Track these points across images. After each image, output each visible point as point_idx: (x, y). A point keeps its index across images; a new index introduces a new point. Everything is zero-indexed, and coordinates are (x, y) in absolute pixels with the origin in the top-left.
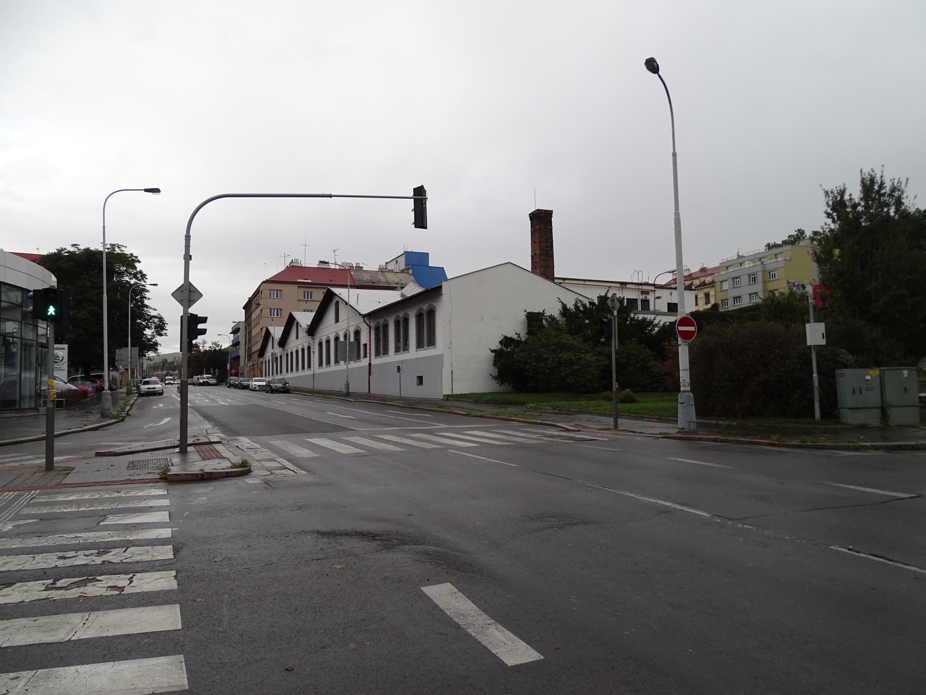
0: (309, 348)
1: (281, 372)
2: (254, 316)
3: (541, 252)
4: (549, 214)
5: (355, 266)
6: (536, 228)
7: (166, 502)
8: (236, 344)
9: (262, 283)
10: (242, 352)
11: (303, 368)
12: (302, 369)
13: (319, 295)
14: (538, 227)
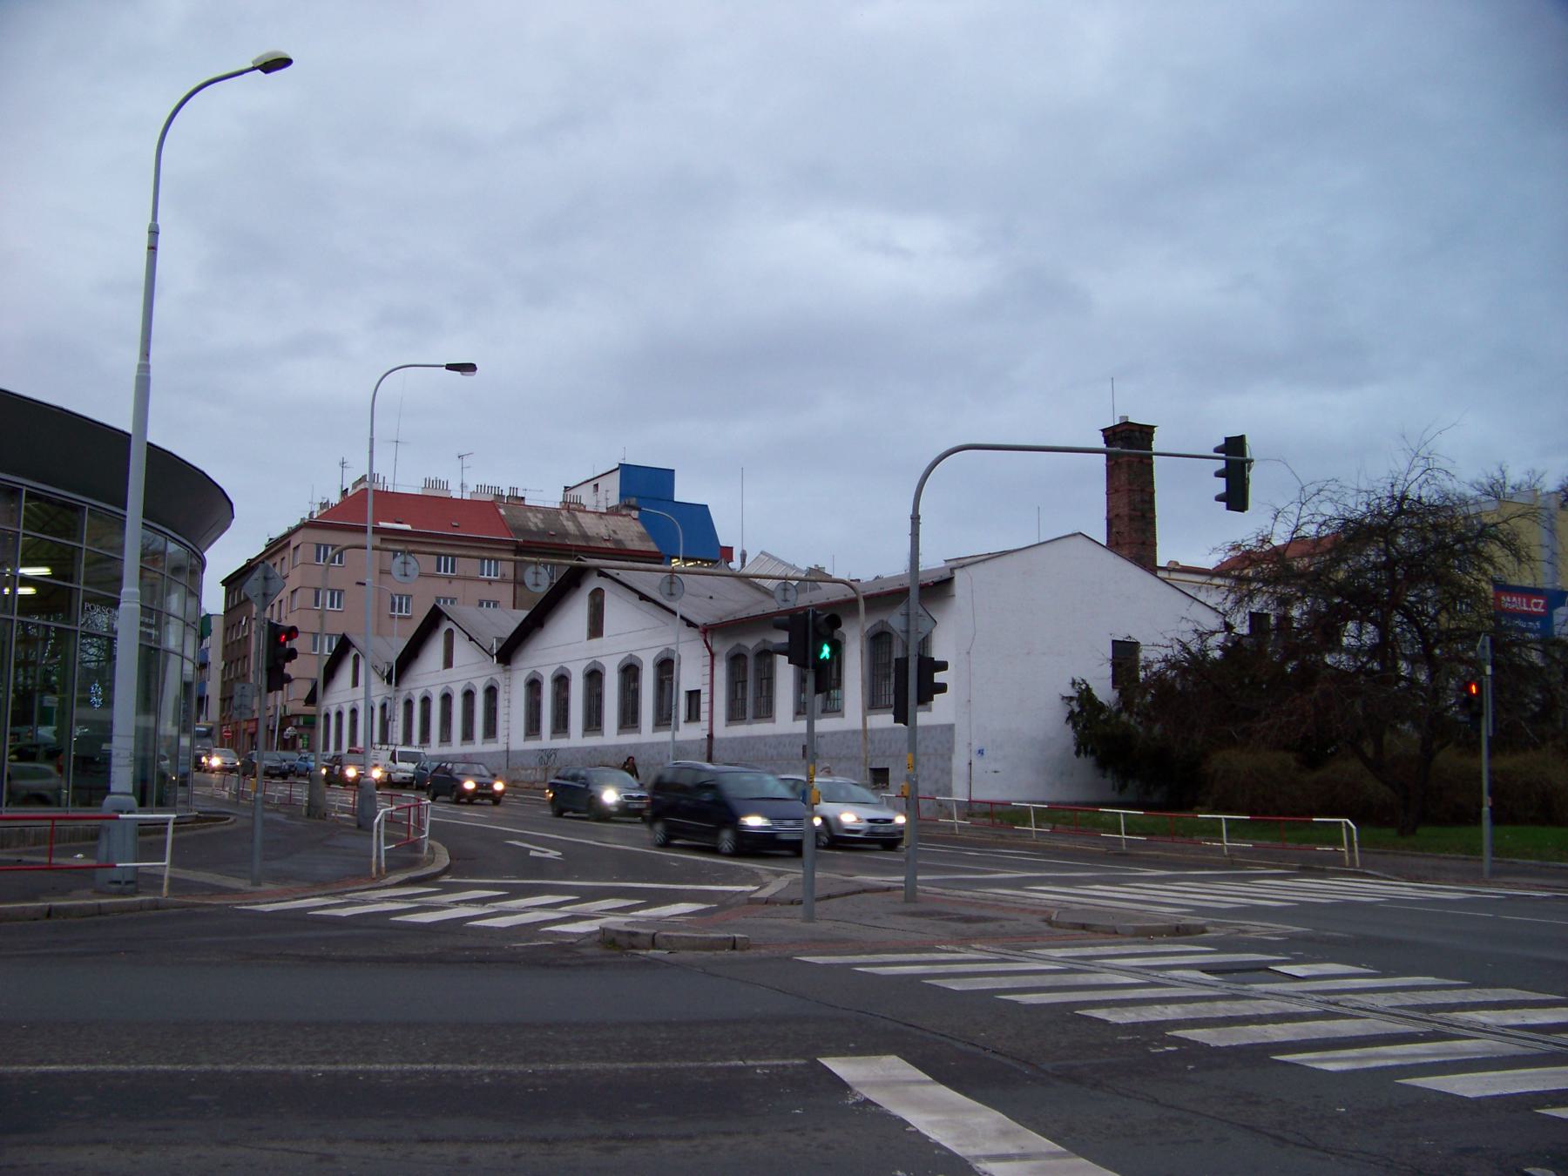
0: (491, 692)
3: (1133, 513)
4: (1147, 433)
5: (506, 493)
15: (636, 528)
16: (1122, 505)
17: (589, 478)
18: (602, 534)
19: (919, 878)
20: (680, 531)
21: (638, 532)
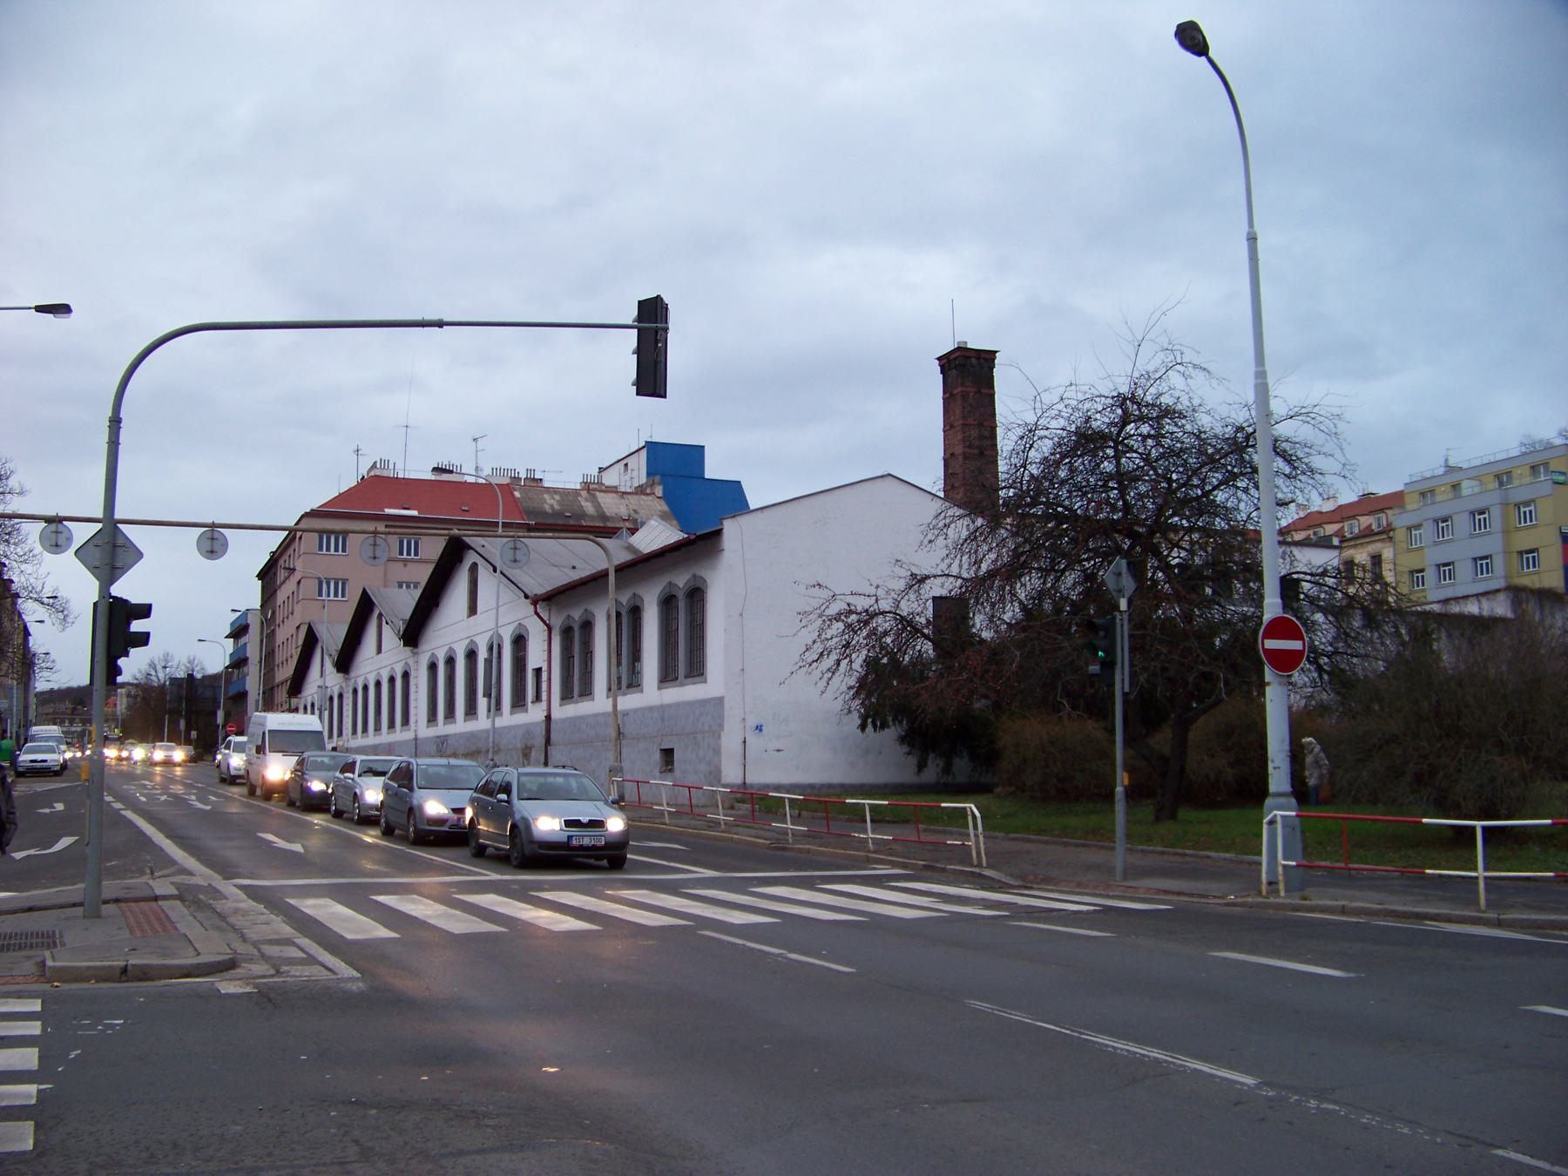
0: (406, 675)
1: (340, 734)
2: (281, 596)
4: (986, 360)
6: (955, 392)
7: (35, 1028)
8: (239, 662)
9: (302, 517)
10: (253, 683)
11: (392, 725)
12: (389, 728)
13: (433, 548)
14: (959, 389)
15: (659, 507)
16: (957, 443)
17: (620, 458)
18: (622, 514)
20: (499, 494)
21: (660, 511)
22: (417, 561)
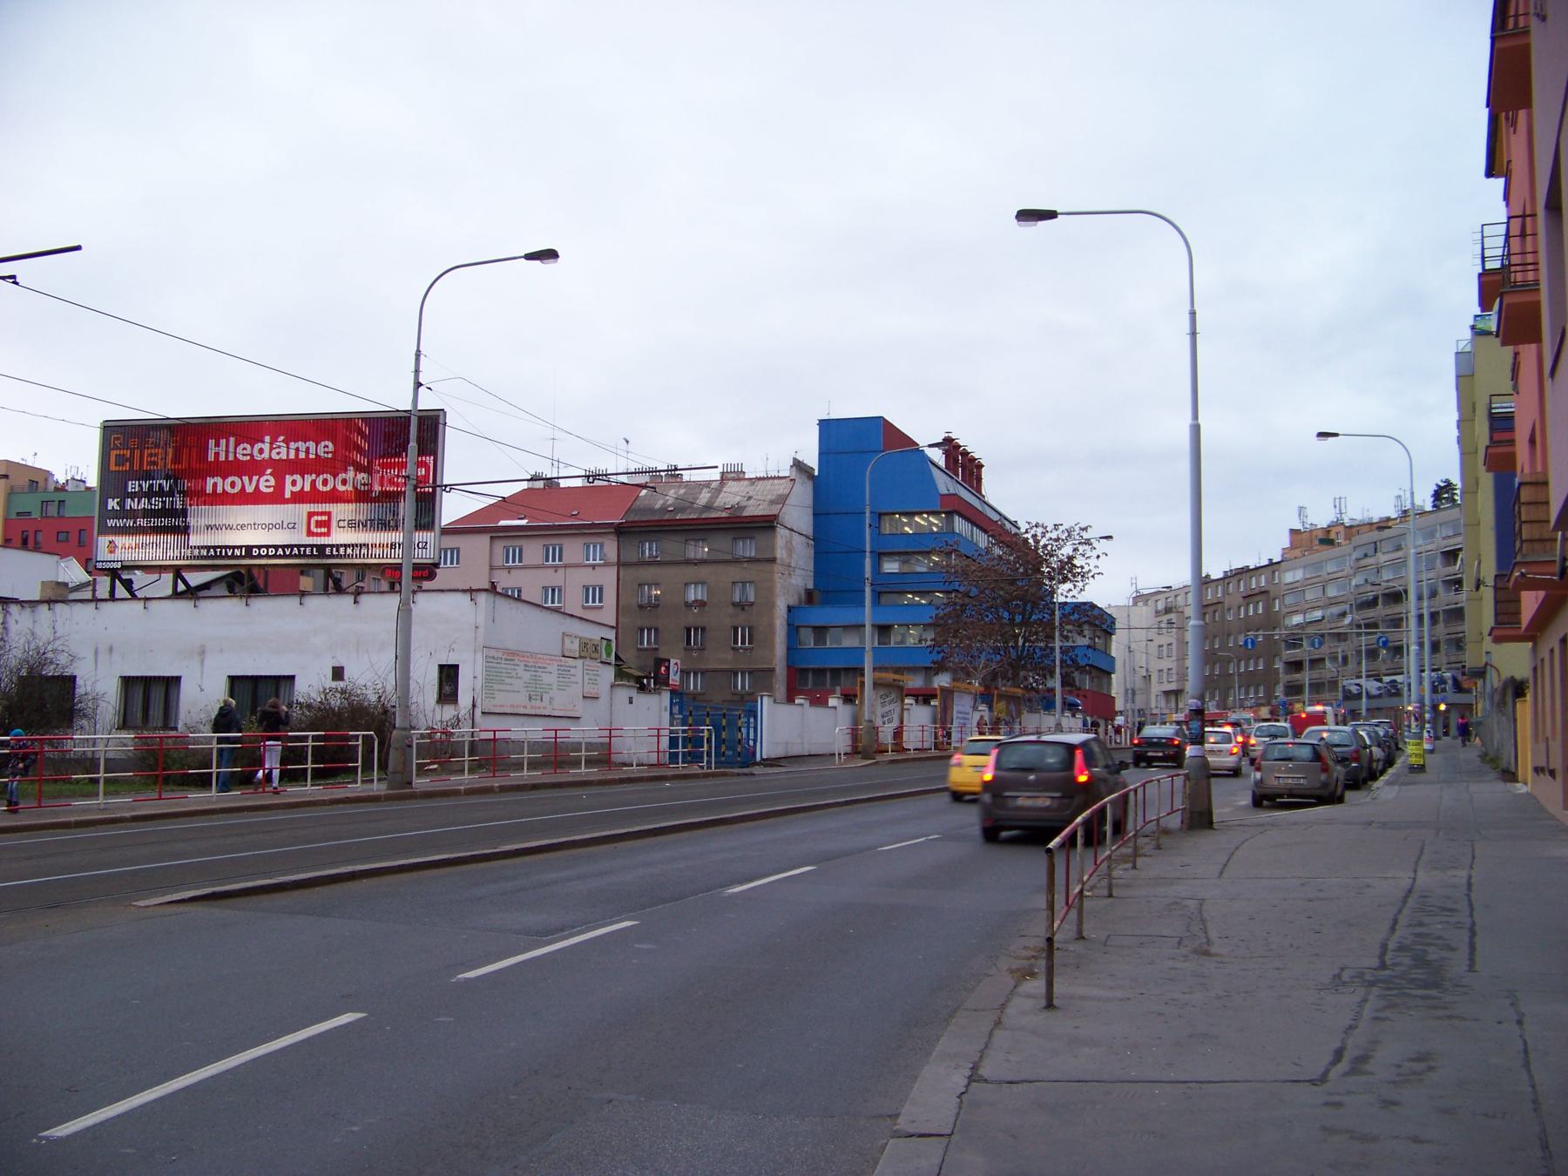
19: (1207, 729)
22: (521, 568)
